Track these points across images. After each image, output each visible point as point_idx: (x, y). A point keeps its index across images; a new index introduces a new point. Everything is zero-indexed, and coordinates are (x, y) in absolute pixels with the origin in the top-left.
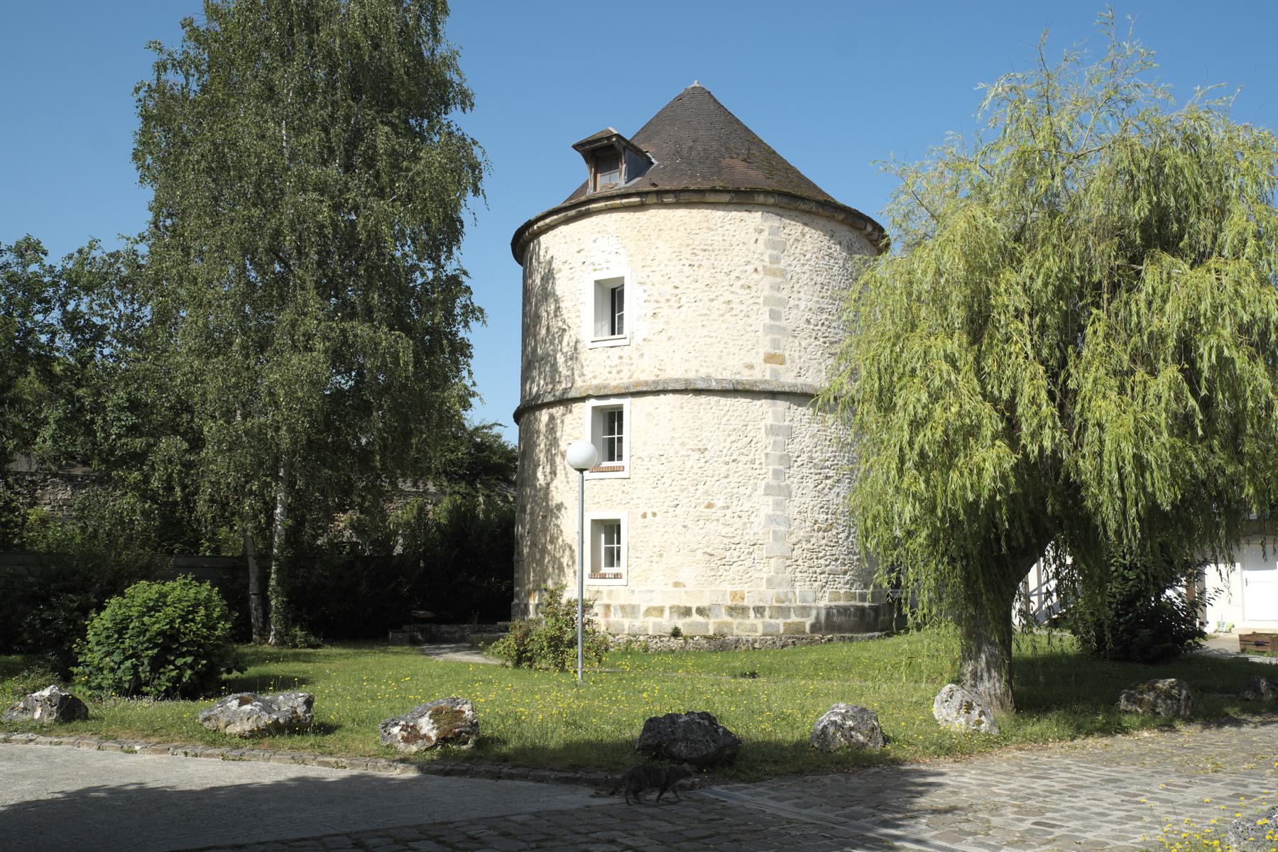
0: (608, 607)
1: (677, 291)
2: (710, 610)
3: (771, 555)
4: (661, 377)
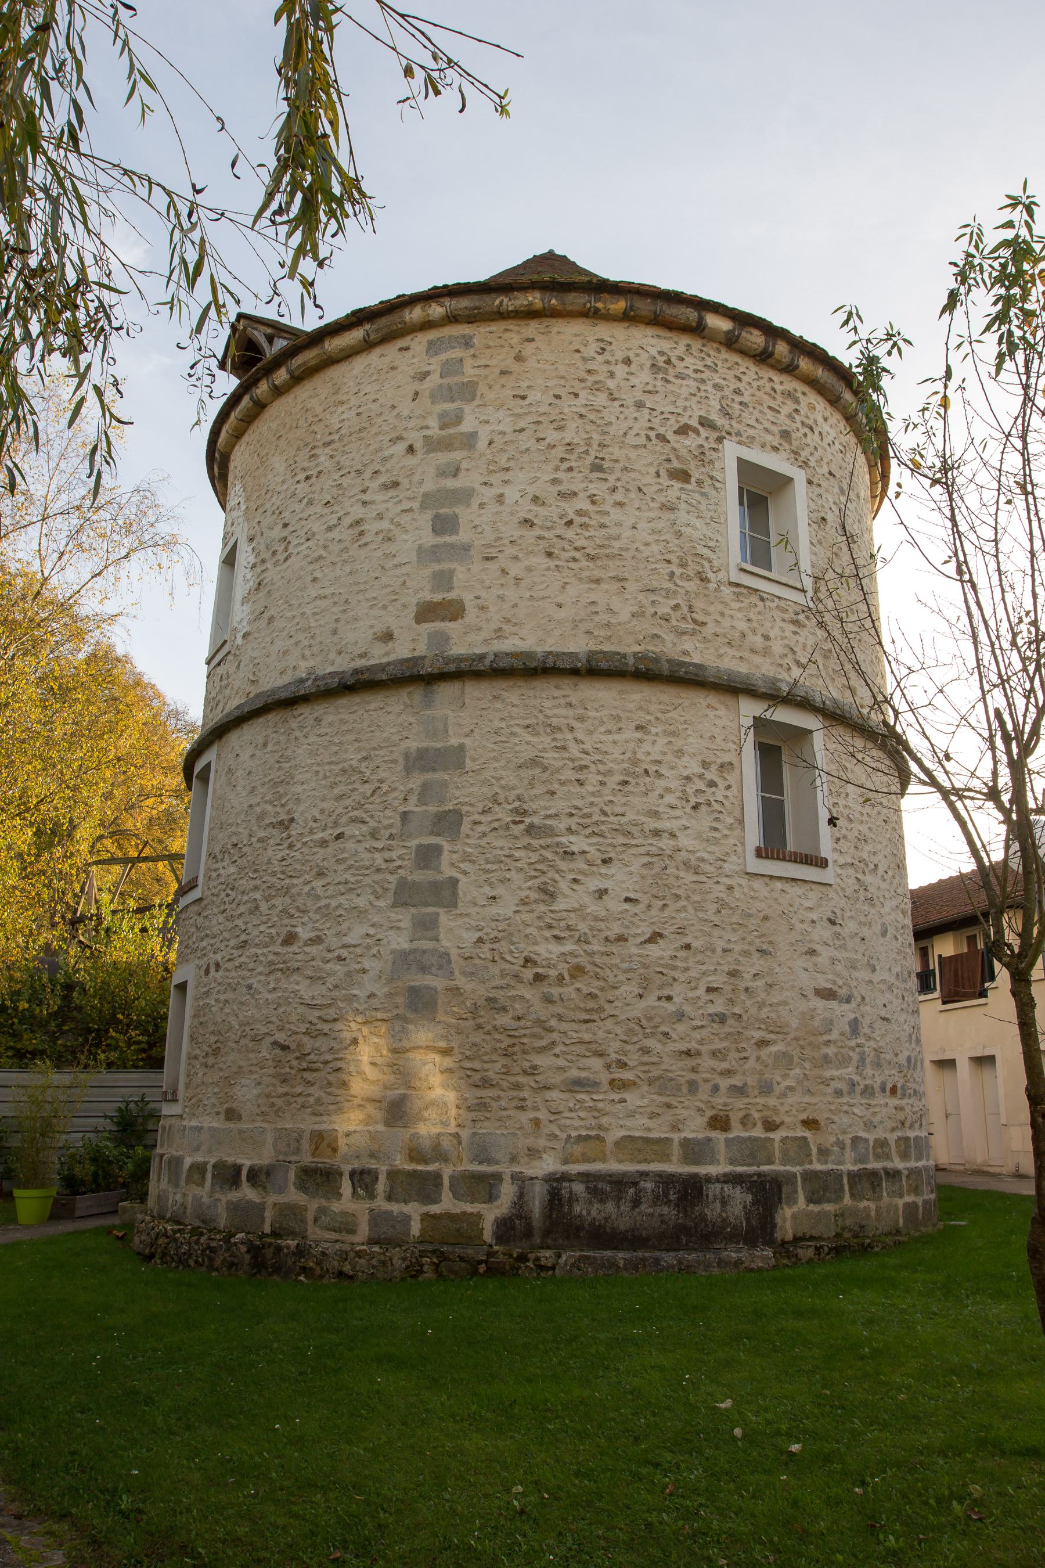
2: (268, 1174)
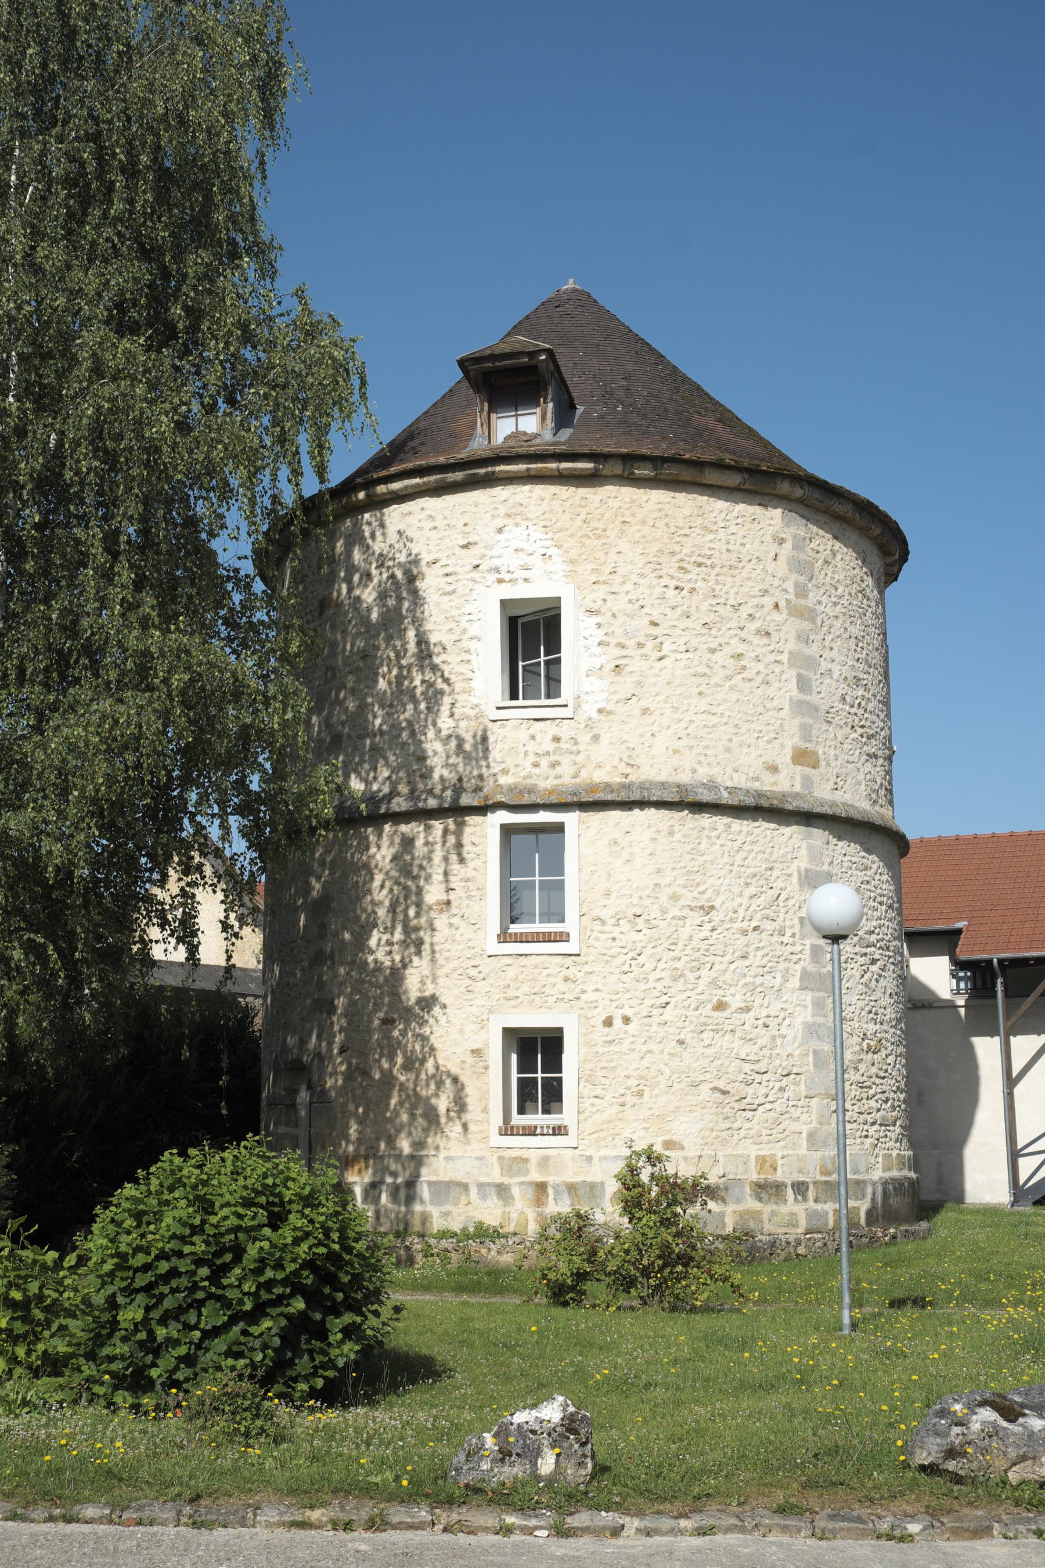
0: (541, 1187)
1: (655, 631)
2: (726, 1189)
4: (633, 778)
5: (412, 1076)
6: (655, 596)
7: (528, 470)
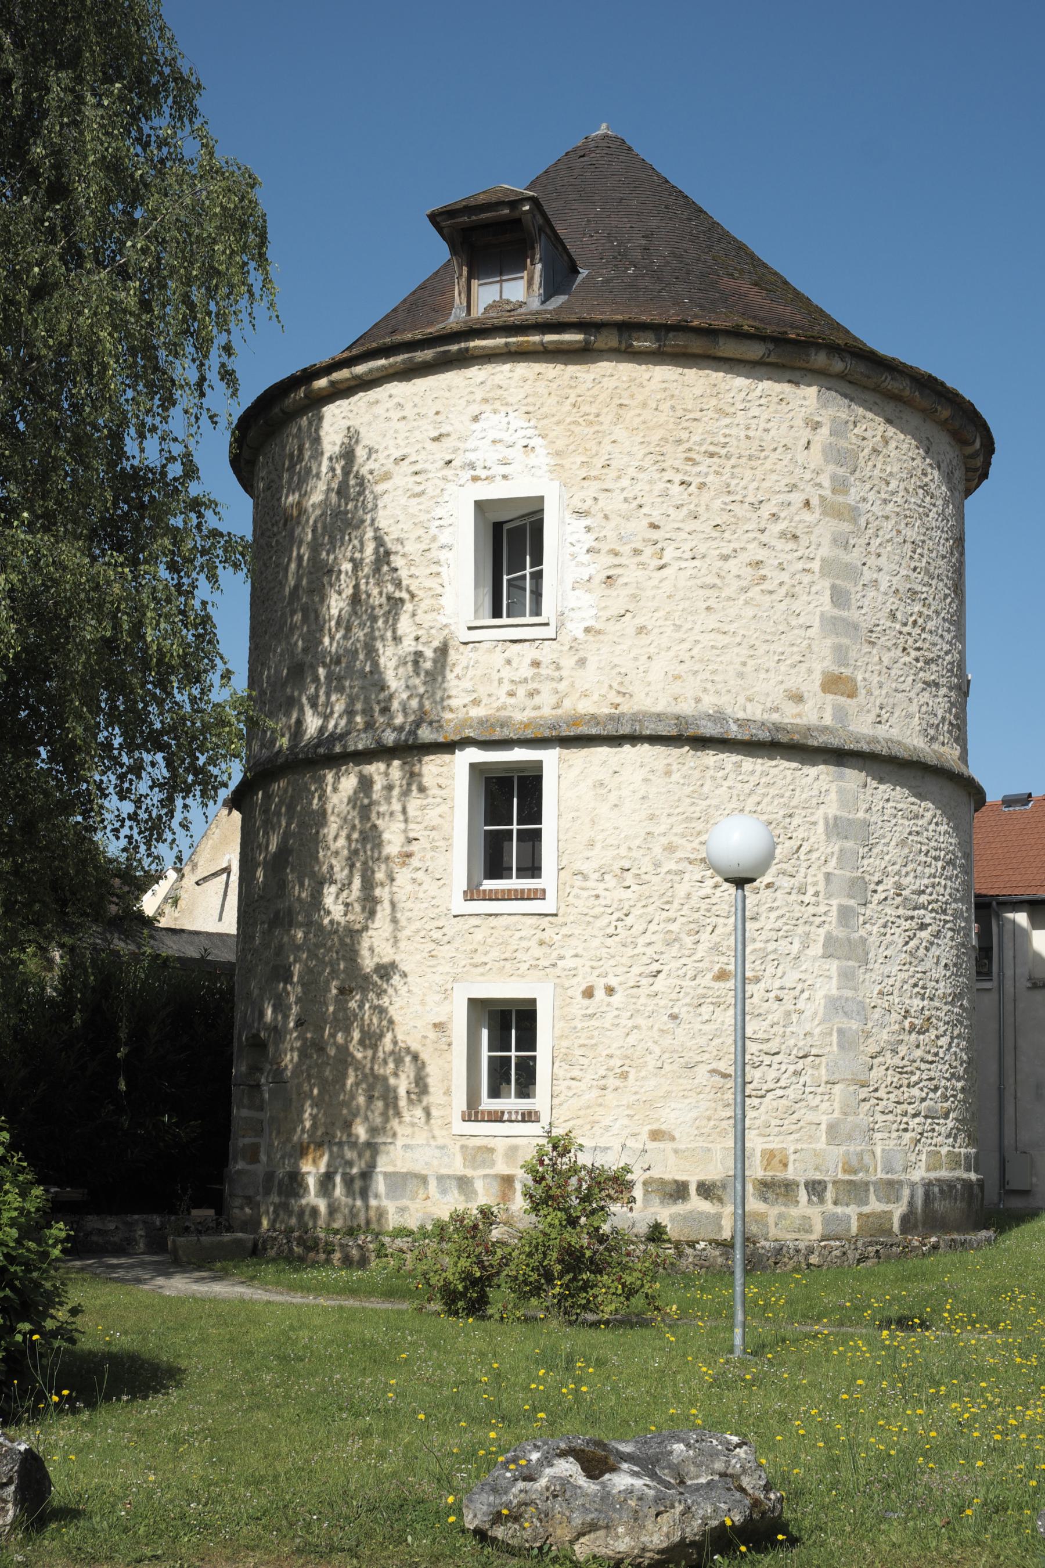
1: (655, 535)
2: (724, 1187)
3: (836, 1077)
4: (624, 708)
5: (369, 1053)
6: (656, 493)
7: (507, 344)
